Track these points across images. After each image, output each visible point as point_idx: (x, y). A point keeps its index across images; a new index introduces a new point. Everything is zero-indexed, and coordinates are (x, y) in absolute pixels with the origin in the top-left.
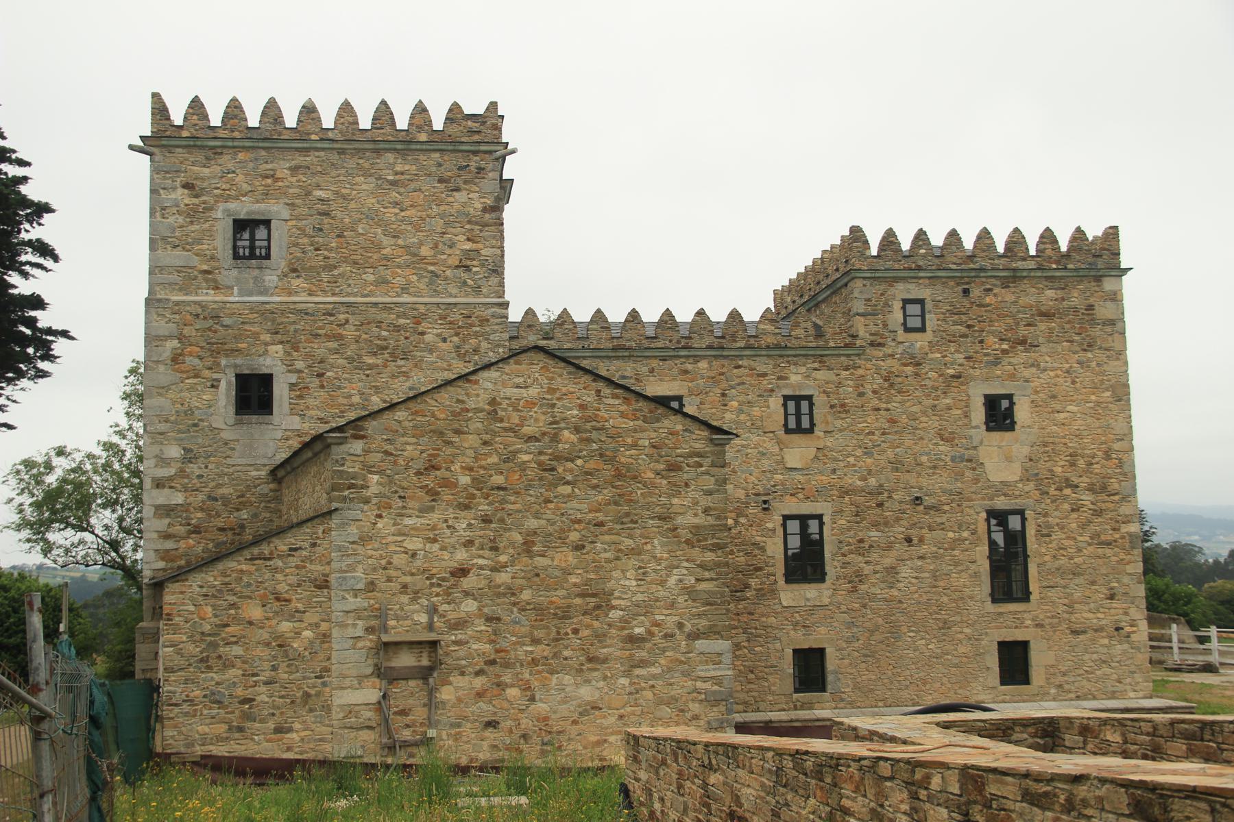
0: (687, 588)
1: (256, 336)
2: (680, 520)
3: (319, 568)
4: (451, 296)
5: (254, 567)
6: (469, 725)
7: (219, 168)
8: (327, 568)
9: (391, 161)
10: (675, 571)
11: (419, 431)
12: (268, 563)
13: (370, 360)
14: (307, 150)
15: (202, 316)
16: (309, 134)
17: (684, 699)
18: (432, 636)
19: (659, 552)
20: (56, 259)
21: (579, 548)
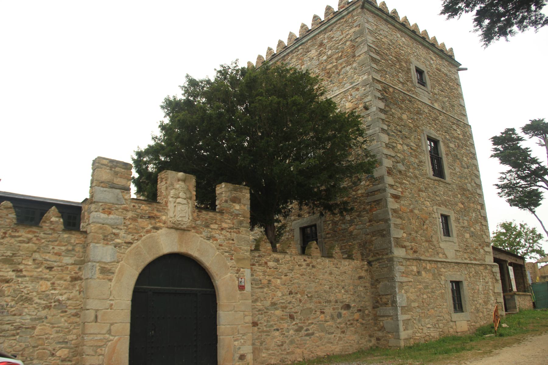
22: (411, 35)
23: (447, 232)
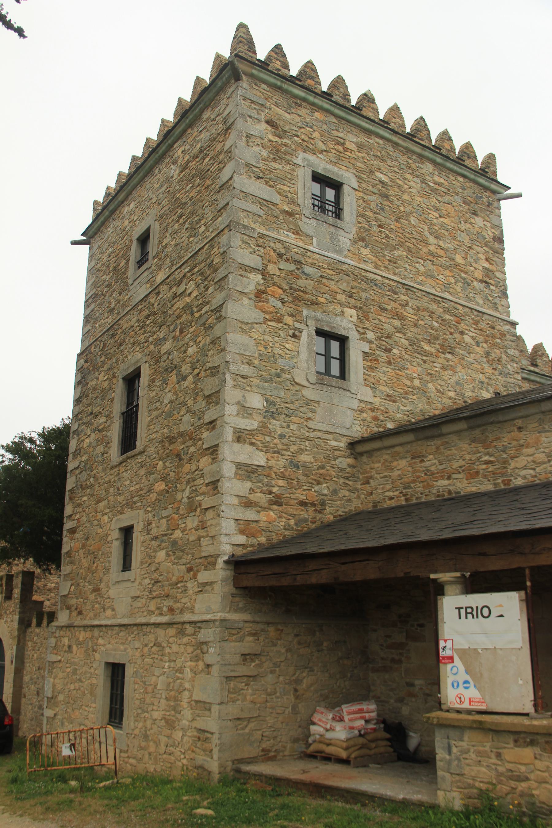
22: (141, 174)
23: (126, 566)
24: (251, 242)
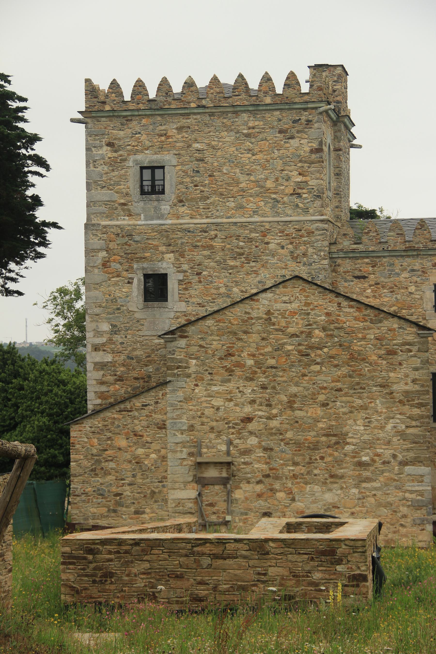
0: (400, 432)
1: (156, 248)
2: (395, 387)
3: (160, 416)
4: (287, 215)
5: (121, 416)
6: (253, 514)
7: (130, 131)
8: (165, 417)
9: (246, 119)
10: (391, 421)
11: (221, 333)
12: (130, 414)
13: (232, 263)
14: (188, 114)
15: (121, 235)
16: (189, 103)
17: (396, 504)
18: (229, 459)
19: (380, 408)
20: (48, 168)
21: (324, 405)
24: (98, 233)
